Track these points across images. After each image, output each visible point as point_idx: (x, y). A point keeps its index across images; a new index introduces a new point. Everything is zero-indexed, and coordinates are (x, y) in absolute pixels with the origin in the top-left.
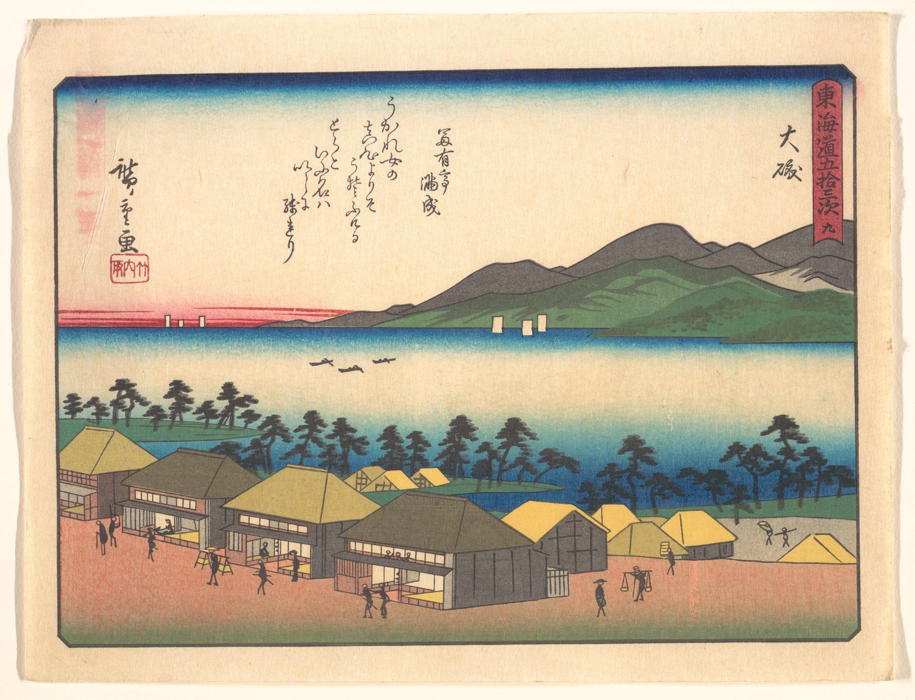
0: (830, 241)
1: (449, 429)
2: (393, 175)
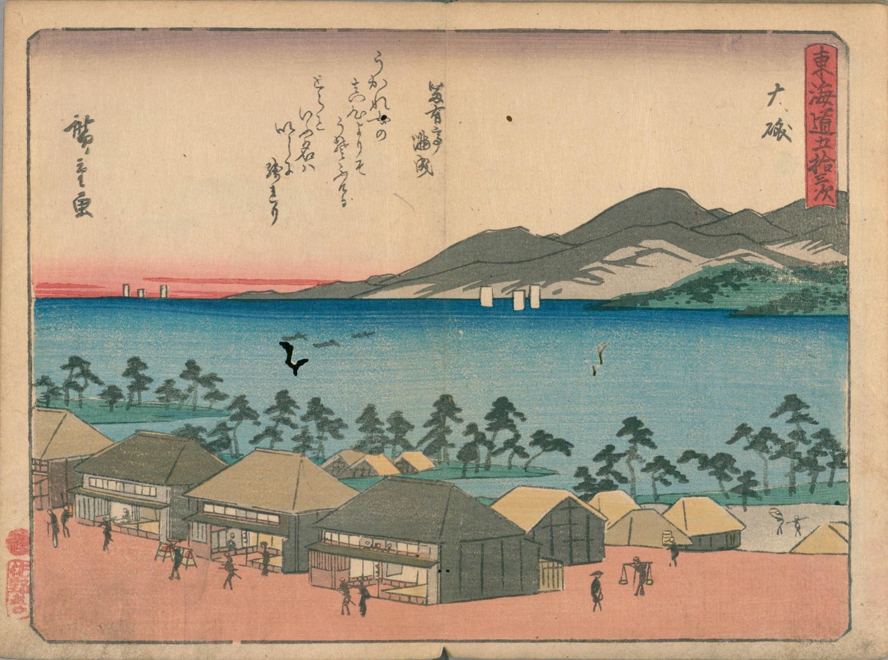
0: (824, 206)
2: (381, 134)
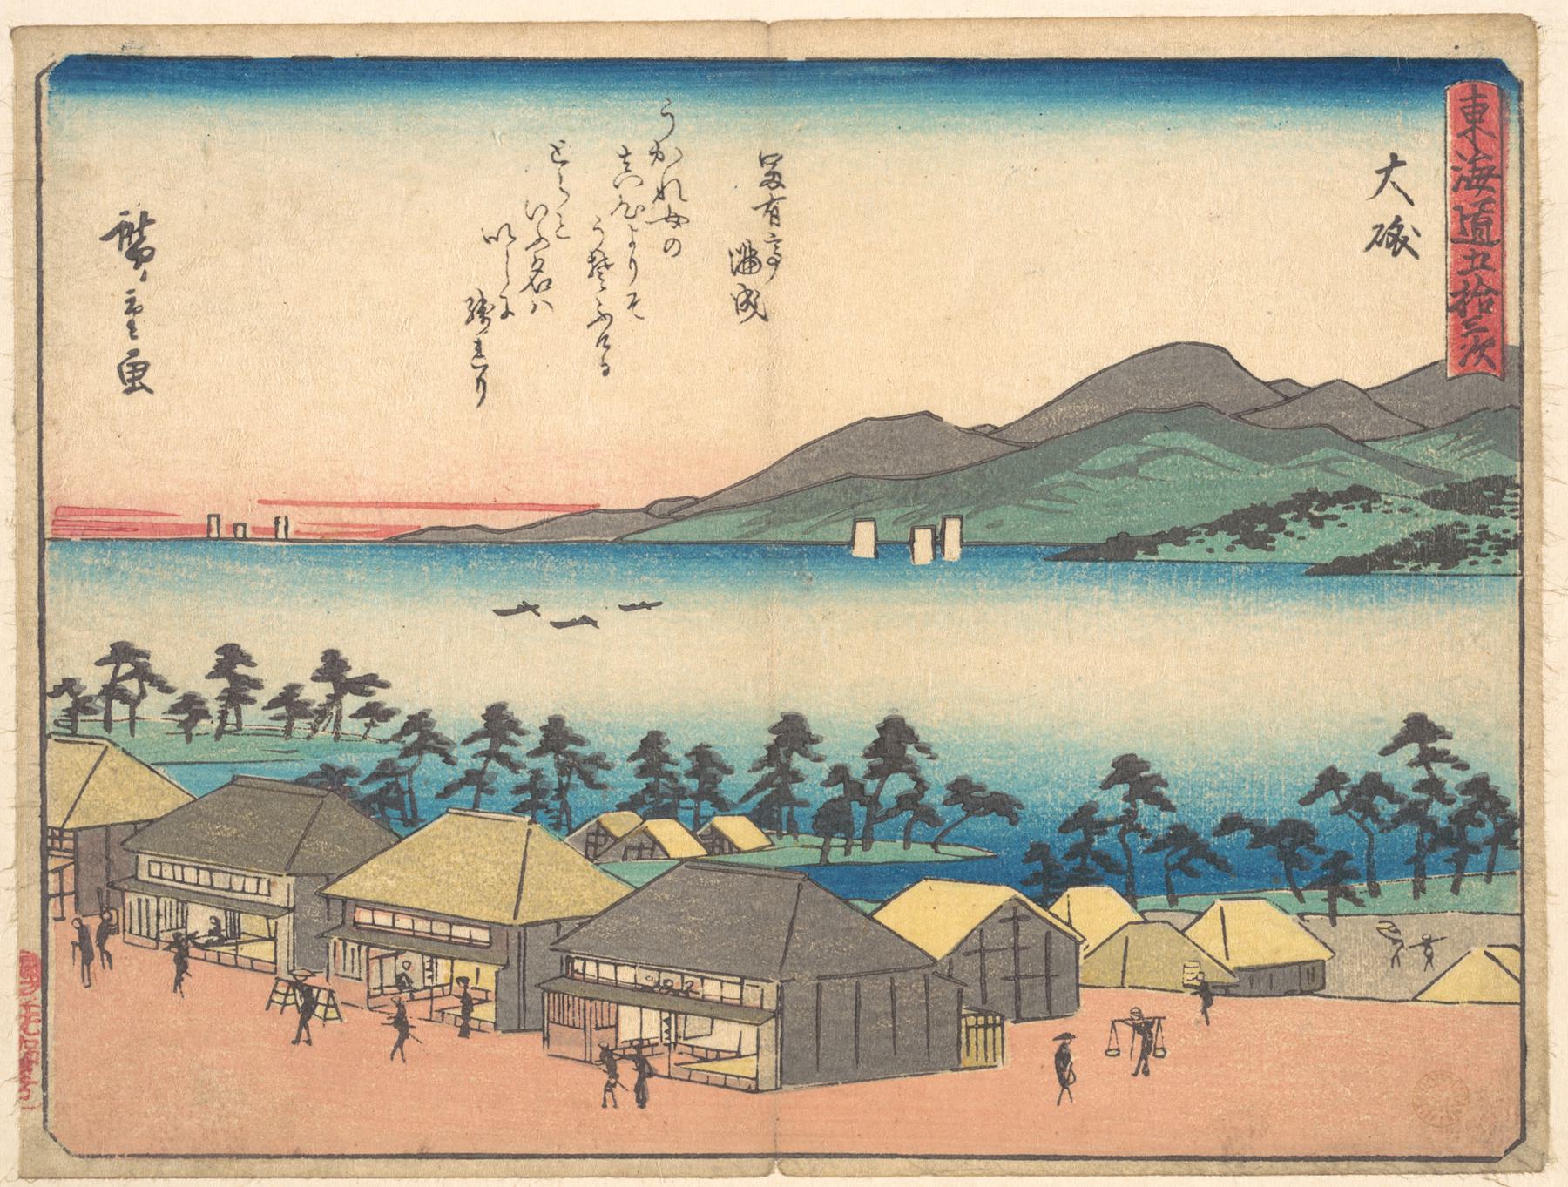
1: (770, 739)
2: (671, 247)
